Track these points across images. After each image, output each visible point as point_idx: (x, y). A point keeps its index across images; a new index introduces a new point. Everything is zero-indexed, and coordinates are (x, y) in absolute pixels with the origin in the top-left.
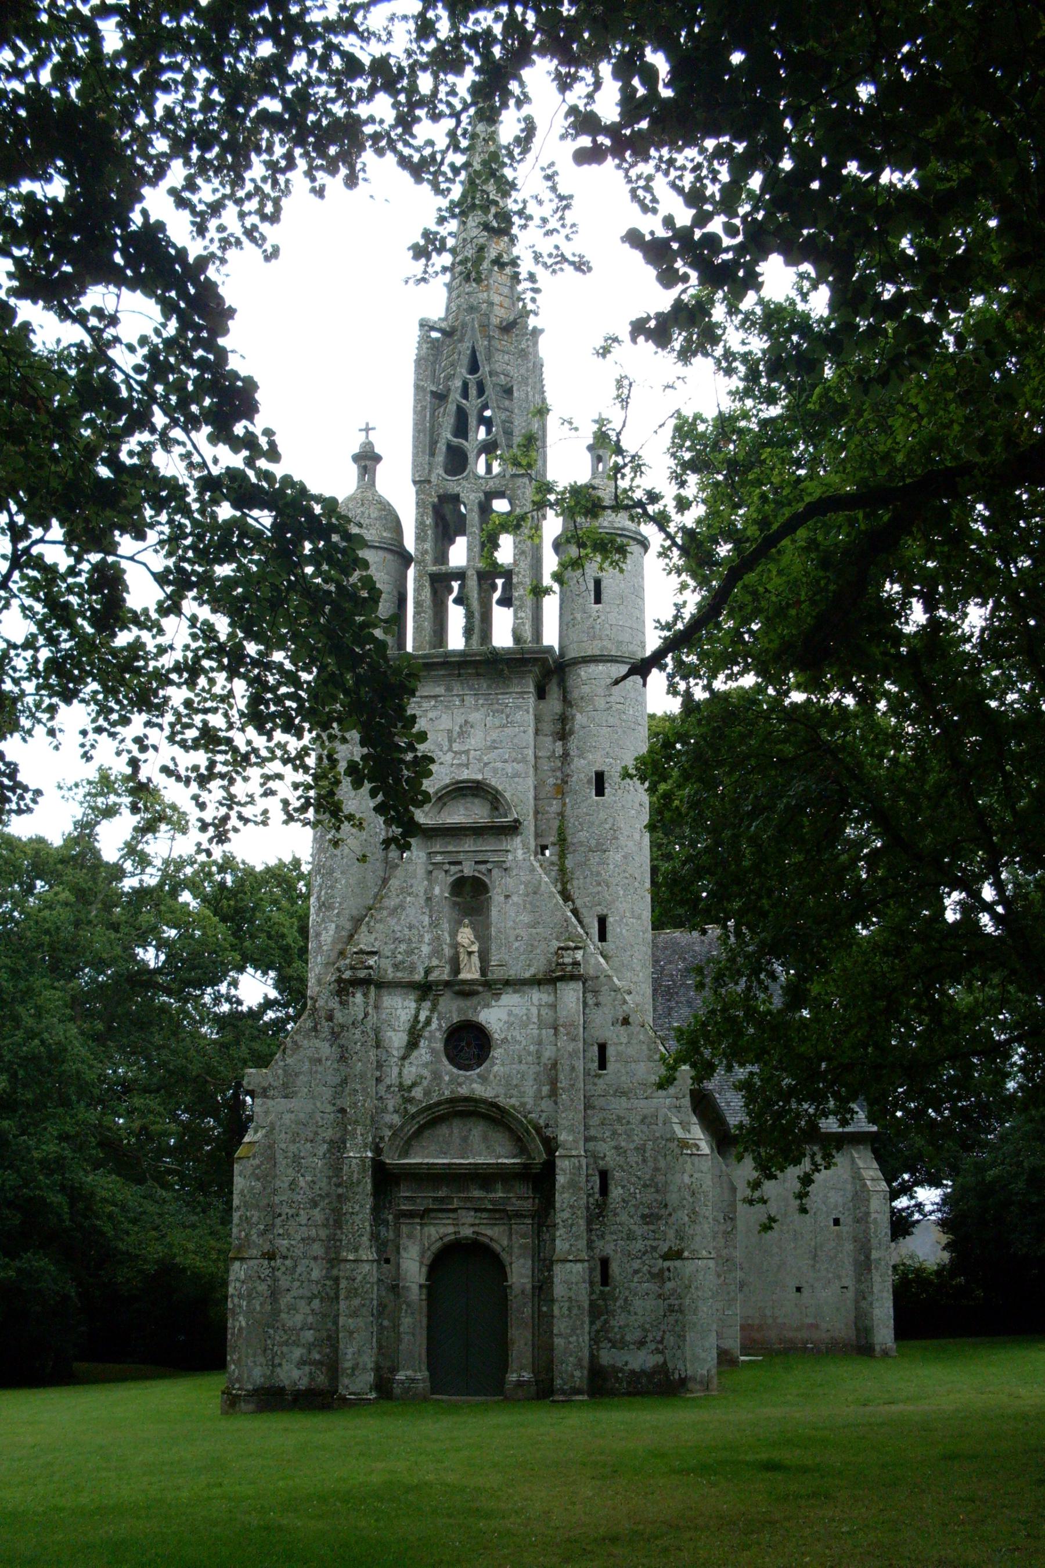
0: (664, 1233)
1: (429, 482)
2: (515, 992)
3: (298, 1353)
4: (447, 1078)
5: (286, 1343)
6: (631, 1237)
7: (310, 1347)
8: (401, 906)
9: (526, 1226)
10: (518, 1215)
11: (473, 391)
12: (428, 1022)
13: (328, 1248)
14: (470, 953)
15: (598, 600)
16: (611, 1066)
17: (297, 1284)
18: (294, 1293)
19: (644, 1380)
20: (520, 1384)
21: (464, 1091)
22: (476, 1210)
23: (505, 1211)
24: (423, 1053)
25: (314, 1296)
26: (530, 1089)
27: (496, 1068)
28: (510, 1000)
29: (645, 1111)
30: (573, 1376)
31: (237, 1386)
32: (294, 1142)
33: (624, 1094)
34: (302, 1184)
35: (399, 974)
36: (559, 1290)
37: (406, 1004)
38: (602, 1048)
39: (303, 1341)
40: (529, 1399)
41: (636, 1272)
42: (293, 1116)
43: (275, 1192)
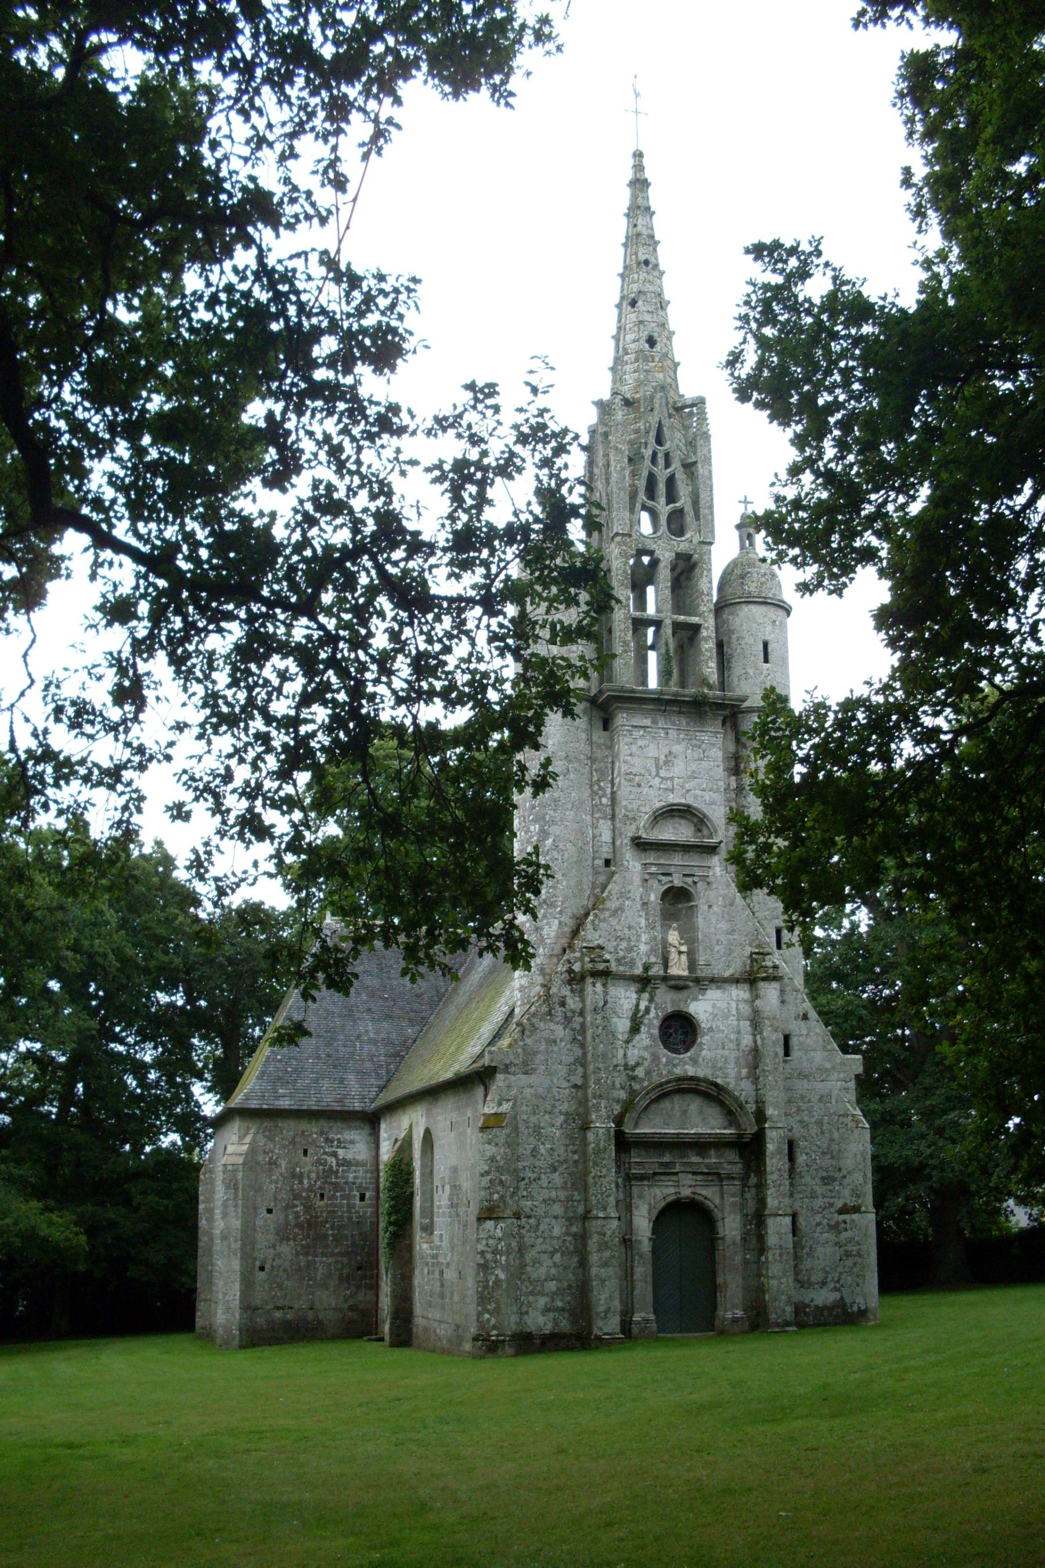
0: (839, 1192)
1: (630, 536)
2: (718, 988)
3: (542, 1301)
4: (664, 1060)
5: (532, 1293)
6: (813, 1195)
7: (553, 1295)
8: (620, 909)
9: (734, 1187)
10: (730, 1177)
11: (661, 461)
12: (647, 1010)
13: (567, 1208)
14: (680, 953)
15: (766, 661)
16: (796, 1054)
17: (540, 1240)
18: (538, 1248)
19: (826, 1313)
20: (735, 1320)
21: (678, 1071)
22: (694, 1173)
23: (719, 1174)
24: (643, 1038)
25: (556, 1251)
26: (732, 1072)
27: (704, 1053)
28: (713, 994)
29: (821, 1092)
30: (784, 1311)
31: (495, 1332)
32: (534, 1113)
33: (806, 1077)
34: (543, 1151)
35: (621, 968)
36: (772, 1240)
37: (628, 994)
38: (787, 1038)
39: (547, 1291)
40: (744, 1332)
41: (818, 1224)
42: (532, 1091)
43: (519, 1158)
